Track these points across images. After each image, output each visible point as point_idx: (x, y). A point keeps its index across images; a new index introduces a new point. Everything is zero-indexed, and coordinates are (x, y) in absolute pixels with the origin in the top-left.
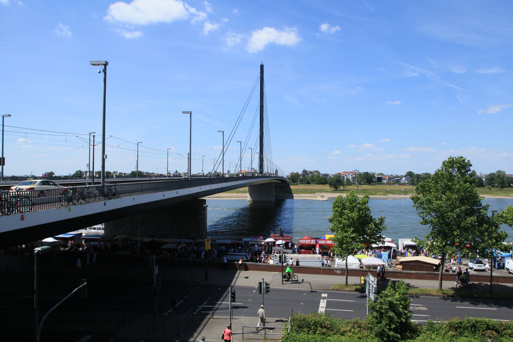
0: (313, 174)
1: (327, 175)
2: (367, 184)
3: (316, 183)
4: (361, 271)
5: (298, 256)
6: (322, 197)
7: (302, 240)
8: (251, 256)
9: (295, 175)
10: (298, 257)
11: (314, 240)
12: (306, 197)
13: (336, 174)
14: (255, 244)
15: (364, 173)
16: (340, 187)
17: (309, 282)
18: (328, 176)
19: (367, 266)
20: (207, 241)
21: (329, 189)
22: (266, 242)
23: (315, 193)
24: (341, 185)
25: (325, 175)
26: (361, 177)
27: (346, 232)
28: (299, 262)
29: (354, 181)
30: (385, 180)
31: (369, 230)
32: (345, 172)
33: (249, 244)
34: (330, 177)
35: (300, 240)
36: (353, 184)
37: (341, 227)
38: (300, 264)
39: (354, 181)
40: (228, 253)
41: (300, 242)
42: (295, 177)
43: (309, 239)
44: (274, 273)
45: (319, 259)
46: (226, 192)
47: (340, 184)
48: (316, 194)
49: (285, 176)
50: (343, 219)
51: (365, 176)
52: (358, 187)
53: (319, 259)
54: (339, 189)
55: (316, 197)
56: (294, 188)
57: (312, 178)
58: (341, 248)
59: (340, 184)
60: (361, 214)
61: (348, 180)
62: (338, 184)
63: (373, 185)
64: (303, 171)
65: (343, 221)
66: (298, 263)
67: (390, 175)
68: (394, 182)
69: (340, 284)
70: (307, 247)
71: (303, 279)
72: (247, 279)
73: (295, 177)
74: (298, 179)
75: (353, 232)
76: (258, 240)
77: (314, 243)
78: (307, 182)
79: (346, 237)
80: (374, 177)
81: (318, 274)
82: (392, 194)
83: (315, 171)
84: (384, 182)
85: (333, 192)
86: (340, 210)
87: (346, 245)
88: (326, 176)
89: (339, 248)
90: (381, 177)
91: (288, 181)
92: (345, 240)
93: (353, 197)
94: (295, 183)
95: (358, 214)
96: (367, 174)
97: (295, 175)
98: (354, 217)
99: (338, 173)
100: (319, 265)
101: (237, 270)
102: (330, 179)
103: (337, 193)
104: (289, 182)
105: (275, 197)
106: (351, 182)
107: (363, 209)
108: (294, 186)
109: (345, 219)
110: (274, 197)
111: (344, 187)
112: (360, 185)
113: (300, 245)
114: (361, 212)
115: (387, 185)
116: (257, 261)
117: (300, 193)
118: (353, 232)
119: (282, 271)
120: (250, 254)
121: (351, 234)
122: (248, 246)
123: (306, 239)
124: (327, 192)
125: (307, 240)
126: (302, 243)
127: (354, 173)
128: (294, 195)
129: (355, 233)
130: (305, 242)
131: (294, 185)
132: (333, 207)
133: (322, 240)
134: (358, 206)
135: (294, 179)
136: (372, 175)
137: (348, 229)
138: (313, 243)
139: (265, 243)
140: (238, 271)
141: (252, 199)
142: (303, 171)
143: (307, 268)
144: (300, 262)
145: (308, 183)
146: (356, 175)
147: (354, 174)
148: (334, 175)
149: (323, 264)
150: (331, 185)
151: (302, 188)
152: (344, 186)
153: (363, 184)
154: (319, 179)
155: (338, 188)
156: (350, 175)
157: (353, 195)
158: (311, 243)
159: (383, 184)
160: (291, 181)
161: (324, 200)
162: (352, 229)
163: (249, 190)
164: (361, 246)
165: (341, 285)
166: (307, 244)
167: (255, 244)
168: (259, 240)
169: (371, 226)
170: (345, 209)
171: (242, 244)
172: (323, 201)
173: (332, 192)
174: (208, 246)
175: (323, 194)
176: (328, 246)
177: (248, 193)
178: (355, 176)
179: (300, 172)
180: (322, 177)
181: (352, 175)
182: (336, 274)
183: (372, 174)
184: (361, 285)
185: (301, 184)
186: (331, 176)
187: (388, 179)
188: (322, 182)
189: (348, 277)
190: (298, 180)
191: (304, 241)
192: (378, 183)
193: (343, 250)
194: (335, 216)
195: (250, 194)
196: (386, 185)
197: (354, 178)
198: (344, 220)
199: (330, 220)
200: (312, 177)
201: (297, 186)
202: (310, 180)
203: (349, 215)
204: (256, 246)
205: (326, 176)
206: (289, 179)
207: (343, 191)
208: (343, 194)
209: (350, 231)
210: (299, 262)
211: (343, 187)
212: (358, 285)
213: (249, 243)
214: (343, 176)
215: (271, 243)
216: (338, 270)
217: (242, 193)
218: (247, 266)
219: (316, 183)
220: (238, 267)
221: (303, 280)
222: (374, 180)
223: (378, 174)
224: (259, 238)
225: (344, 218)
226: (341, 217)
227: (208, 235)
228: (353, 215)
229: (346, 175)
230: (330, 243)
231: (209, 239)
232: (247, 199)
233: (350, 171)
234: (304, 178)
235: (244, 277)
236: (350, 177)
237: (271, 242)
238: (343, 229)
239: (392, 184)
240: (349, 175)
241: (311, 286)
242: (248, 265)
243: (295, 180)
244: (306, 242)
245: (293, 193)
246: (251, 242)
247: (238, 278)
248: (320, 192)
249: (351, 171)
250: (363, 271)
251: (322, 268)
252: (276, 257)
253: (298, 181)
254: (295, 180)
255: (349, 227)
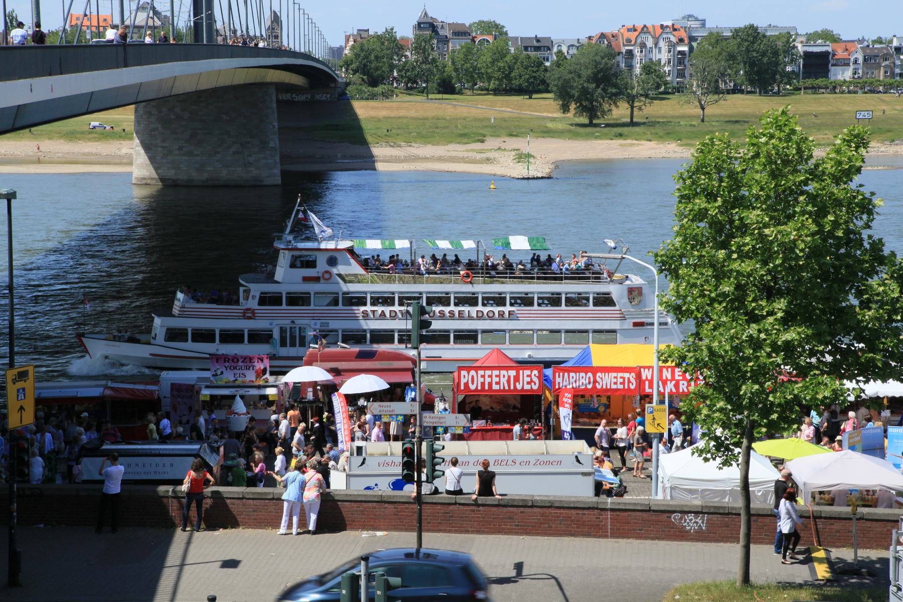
0: (473, 40)
1: (541, 45)
2: (749, 92)
3: (487, 90)
4: (809, 517)
5: (473, 452)
6: (523, 157)
7: (473, 373)
8: (226, 457)
9: (377, 46)
10: (470, 454)
11: (535, 372)
12: (441, 159)
13: (590, 38)
14: (233, 397)
15: (737, 32)
16: (613, 107)
17: (554, 577)
18: (549, 49)
19: (817, 496)
20: (14, 381)
21: (553, 119)
22: (286, 384)
23: (483, 141)
24: (616, 95)
25: (535, 44)
26: (720, 54)
27: (753, 318)
28: (492, 475)
29: (683, 76)
30: (848, 65)
31: (870, 309)
32: (634, 29)
33: (202, 398)
34: (560, 52)
35: (464, 373)
36: (679, 89)
37: (725, 295)
38: (500, 487)
39: (683, 76)
40: (104, 447)
41: (463, 381)
42: (377, 57)
43: (507, 368)
44: (365, 534)
45: (578, 461)
46: (8, 135)
47: (614, 91)
48: (492, 143)
49: (319, 53)
50: (735, 256)
51: (739, 45)
52: (703, 109)
53: (578, 461)
54: (608, 119)
55: (488, 160)
56: (373, 113)
57: (466, 60)
58: (728, 400)
59: (614, 91)
60: (828, 228)
61: (650, 68)
62: (599, 91)
63: (782, 96)
64: (419, 26)
65: (735, 266)
66: (487, 480)
67: (874, 42)
68: (893, 75)
69: (709, 580)
70: (497, 408)
71: (212, 593)
72: (231, 570)
73: (377, 57)
74: (392, 67)
75: (787, 321)
76: (248, 379)
77: (535, 387)
78: (439, 84)
79: (756, 344)
80: (789, 49)
81: (588, 535)
82: (883, 142)
83: (481, 22)
84: (840, 77)
85: (574, 132)
86: (719, 207)
87: (756, 387)
88: (537, 49)
89: (719, 400)
90: (824, 49)
91: (342, 75)
92: (748, 359)
93: (788, 139)
94: (380, 89)
95: (814, 228)
96: (751, 35)
97: (377, 46)
98: (795, 241)
99: (603, 36)
100: (583, 491)
101: (171, 527)
102: (558, 65)
103: (596, 138)
104: (347, 84)
105: (282, 162)
106: (666, 83)
107: (838, 203)
108: (372, 103)
109: (743, 256)
110: (277, 159)
111: (632, 107)
112: (716, 97)
113: (460, 398)
114: (831, 218)
115: (855, 92)
116: (252, 482)
117: (409, 142)
118: (787, 321)
119: (420, 521)
120: (222, 449)
121: (779, 330)
122: (190, 409)
123: (492, 368)
124: (547, 133)
125: (496, 372)
126: (473, 387)
127: (684, 35)
128: (377, 151)
129: (800, 326)
130: (488, 380)
131: (373, 97)
132: (682, 197)
133: (576, 369)
134: (812, 187)
135: (373, 66)
136: (780, 44)
137: (764, 303)
138: (527, 387)
139: (281, 393)
140: (179, 531)
141: (156, 169)
142: (419, 24)
143: (532, 507)
144: (497, 477)
145: (446, 87)
146: (694, 44)
147: (681, 41)
148: (580, 46)
149: (599, 488)
150: (565, 97)
151: (413, 114)
152: (631, 99)
153: (729, 92)
154: (501, 64)
155: (604, 113)
156: (662, 44)
157: (787, 130)
158: (519, 387)
159: (834, 88)
160: (356, 78)
161: (532, 173)
162: (781, 304)
163: (138, 121)
164: (833, 390)
165: (716, 586)
166: (499, 390)
167: (233, 397)
168: (251, 376)
169: (881, 289)
170: (739, 202)
171: (159, 399)
172: (528, 179)
173: (570, 131)
174: (22, 408)
175: (524, 144)
176: (604, 400)
177: (137, 141)
178: (691, 49)
179: (405, 31)
180: (516, 58)
181: (672, 46)
182: (682, 535)
183: (778, 37)
184: (820, 587)
185: (409, 90)
186: (564, 49)
187: (861, 61)
188: (516, 83)
189: (753, 547)
190: (395, 74)
191: (483, 376)
192: (809, 82)
193: (738, 408)
194: (693, 241)
195: (147, 147)
196: (849, 92)
197: (681, 62)
198: (739, 257)
199: (664, 263)
200: (468, 52)
201: (387, 103)
202: (454, 74)
203: (767, 231)
204: (240, 406)
205: (537, 49)
206: (347, 64)
207: (625, 130)
208: (629, 141)
209: (771, 313)
210: (492, 475)
211: (626, 105)
212: (801, 586)
213: (198, 392)
214: (624, 50)
215: (315, 392)
216: (691, 516)
217: (99, 140)
218: (226, 506)
219: (487, 90)
220: (174, 510)
221: (519, 567)
222: (789, 69)
223: (812, 37)
224: (248, 368)
225: (739, 250)
226: (724, 245)
227: (17, 353)
228: (789, 234)
229: (643, 46)
230: (614, 387)
231: (27, 372)
232: (130, 174)
233: (665, 24)
234: (425, 61)
235: (220, 564)
236: (663, 55)
237: (314, 384)
238: (736, 302)
239: (881, 88)
240: (656, 44)
241: (567, 594)
242: (228, 501)
243: (377, 69)
244: (495, 379)
245: (369, 139)
246: (207, 387)
247: (186, 568)
248: (511, 135)
249: (670, 23)
250: (820, 518)
251: (609, 506)
252: (360, 459)
253: (394, 78)
254: (379, 72)
255: (770, 293)
